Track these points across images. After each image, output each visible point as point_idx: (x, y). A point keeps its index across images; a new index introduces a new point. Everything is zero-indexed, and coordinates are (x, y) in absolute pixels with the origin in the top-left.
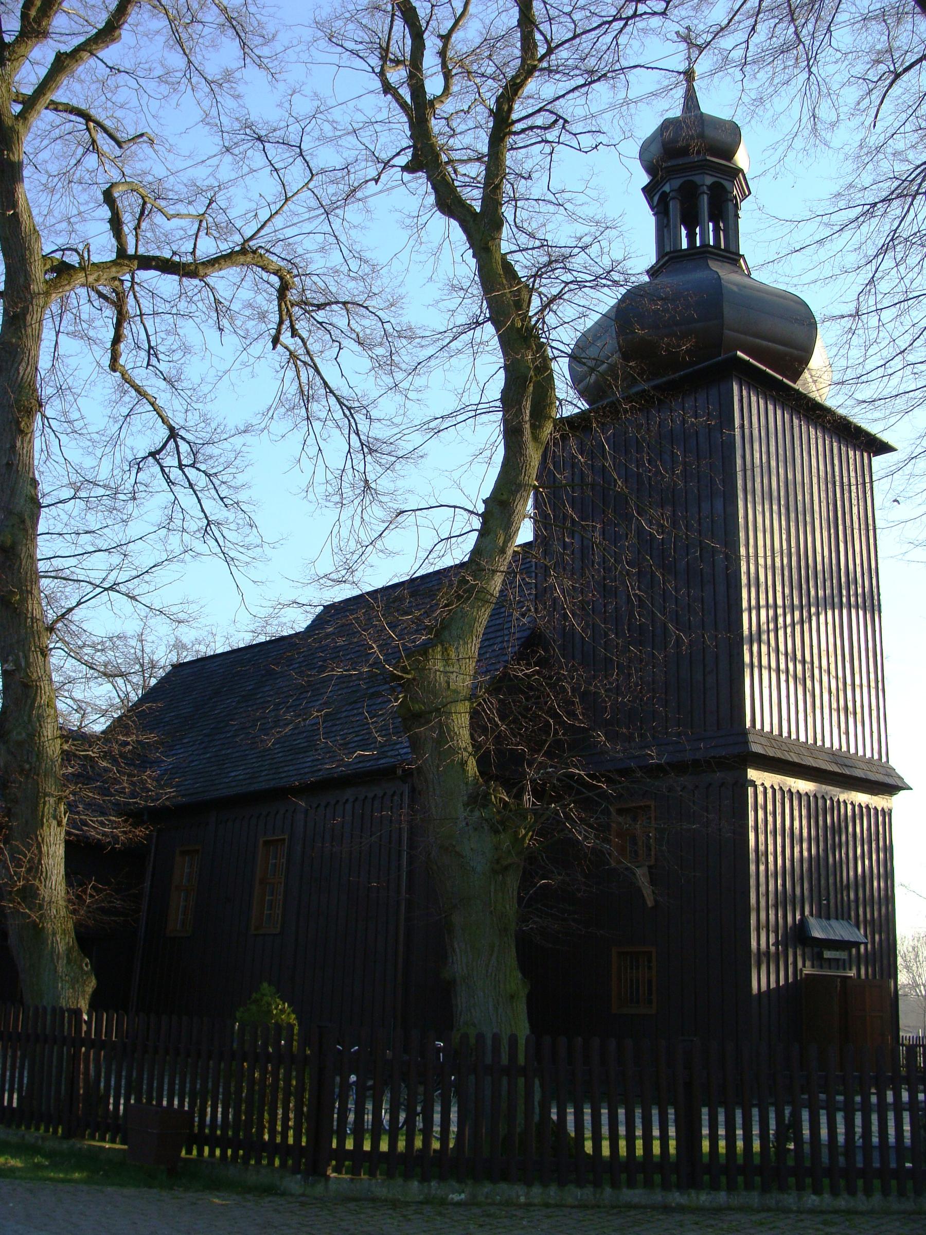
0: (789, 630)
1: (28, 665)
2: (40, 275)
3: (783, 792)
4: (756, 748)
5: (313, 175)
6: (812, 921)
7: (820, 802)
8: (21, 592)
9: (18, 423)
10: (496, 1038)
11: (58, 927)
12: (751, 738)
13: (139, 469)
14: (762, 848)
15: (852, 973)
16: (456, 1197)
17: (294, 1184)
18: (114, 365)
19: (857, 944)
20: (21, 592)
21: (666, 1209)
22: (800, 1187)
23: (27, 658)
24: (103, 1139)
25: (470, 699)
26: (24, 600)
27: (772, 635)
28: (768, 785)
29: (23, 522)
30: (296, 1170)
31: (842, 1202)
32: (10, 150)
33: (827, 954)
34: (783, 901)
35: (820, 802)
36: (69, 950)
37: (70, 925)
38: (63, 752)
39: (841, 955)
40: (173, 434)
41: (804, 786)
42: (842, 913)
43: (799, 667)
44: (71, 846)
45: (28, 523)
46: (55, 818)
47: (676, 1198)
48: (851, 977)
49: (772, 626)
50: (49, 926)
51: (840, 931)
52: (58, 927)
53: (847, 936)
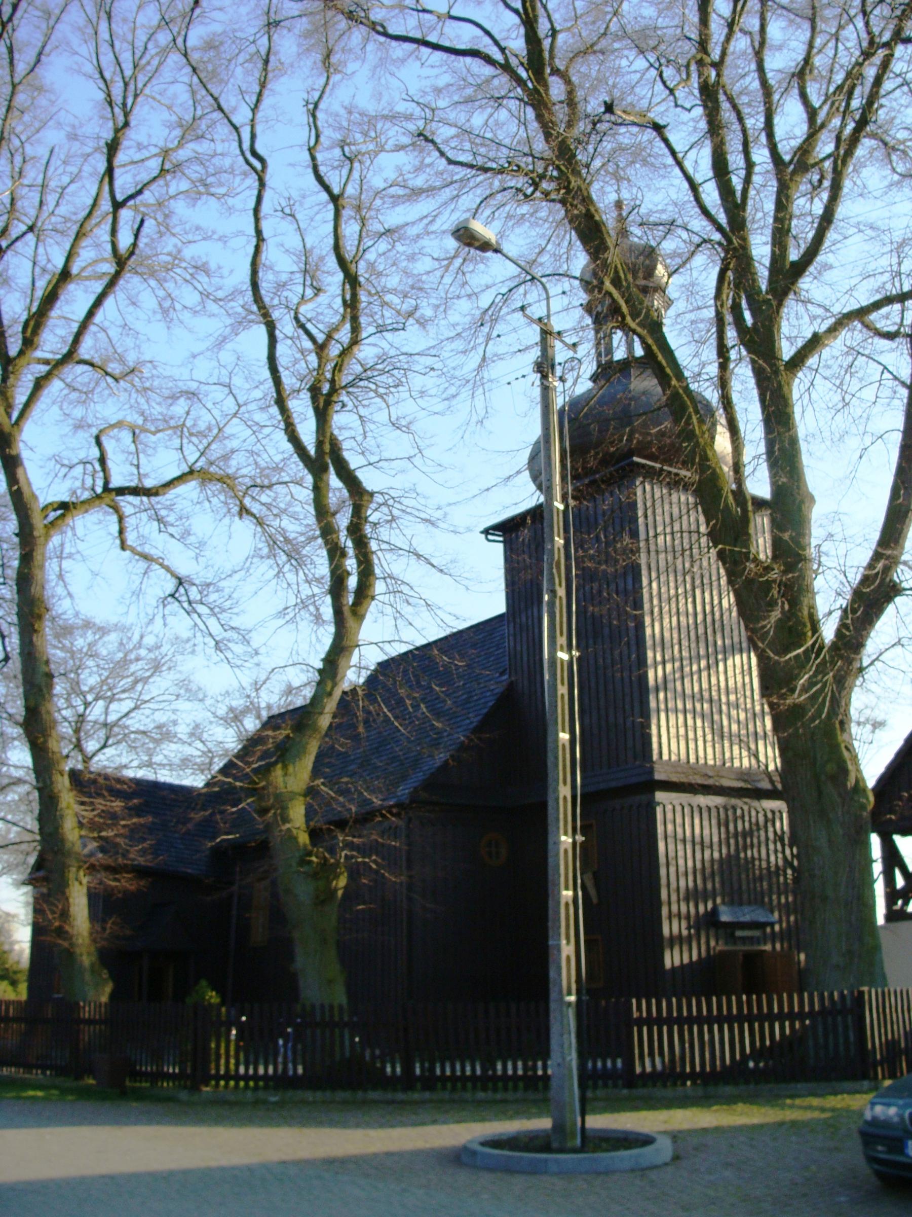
0: (695, 677)
1: (52, 783)
2: (38, 522)
3: (692, 808)
4: (658, 776)
5: (239, 406)
6: (723, 909)
7: (730, 813)
8: (44, 736)
9: (33, 626)
10: (322, 1006)
11: (84, 950)
12: (657, 767)
13: (164, 606)
14: (671, 854)
15: (768, 947)
16: (273, 1099)
17: (184, 1095)
18: (123, 546)
19: (772, 925)
20: (44, 736)
21: (392, 1102)
22: (474, 1088)
23: (50, 778)
24: (140, 1082)
25: (305, 795)
26: (46, 742)
27: (678, 684)
28: (676, 803)
29: (41, 690)
30: (185, 1087)
31: (499, 1096)
32: (10, 447)
33: (739, 933)
34: (693, 895)
35: (730, 813)
36: (92, 965)
37: (93, 949)
38: (81, 837)
39: (756, 933)
40: (180, 582)
41: (718, 800)
42: (758, 900)
43: (706, 706)
44: (92, 897)
45: (45, 691)
46: (77, 879)
47: (400, 1096)
48: (765, 951)
49: (677, 675)
50: (78, 951)
51: (748, 915)
52: (84, 950)
53: (762, 919)
